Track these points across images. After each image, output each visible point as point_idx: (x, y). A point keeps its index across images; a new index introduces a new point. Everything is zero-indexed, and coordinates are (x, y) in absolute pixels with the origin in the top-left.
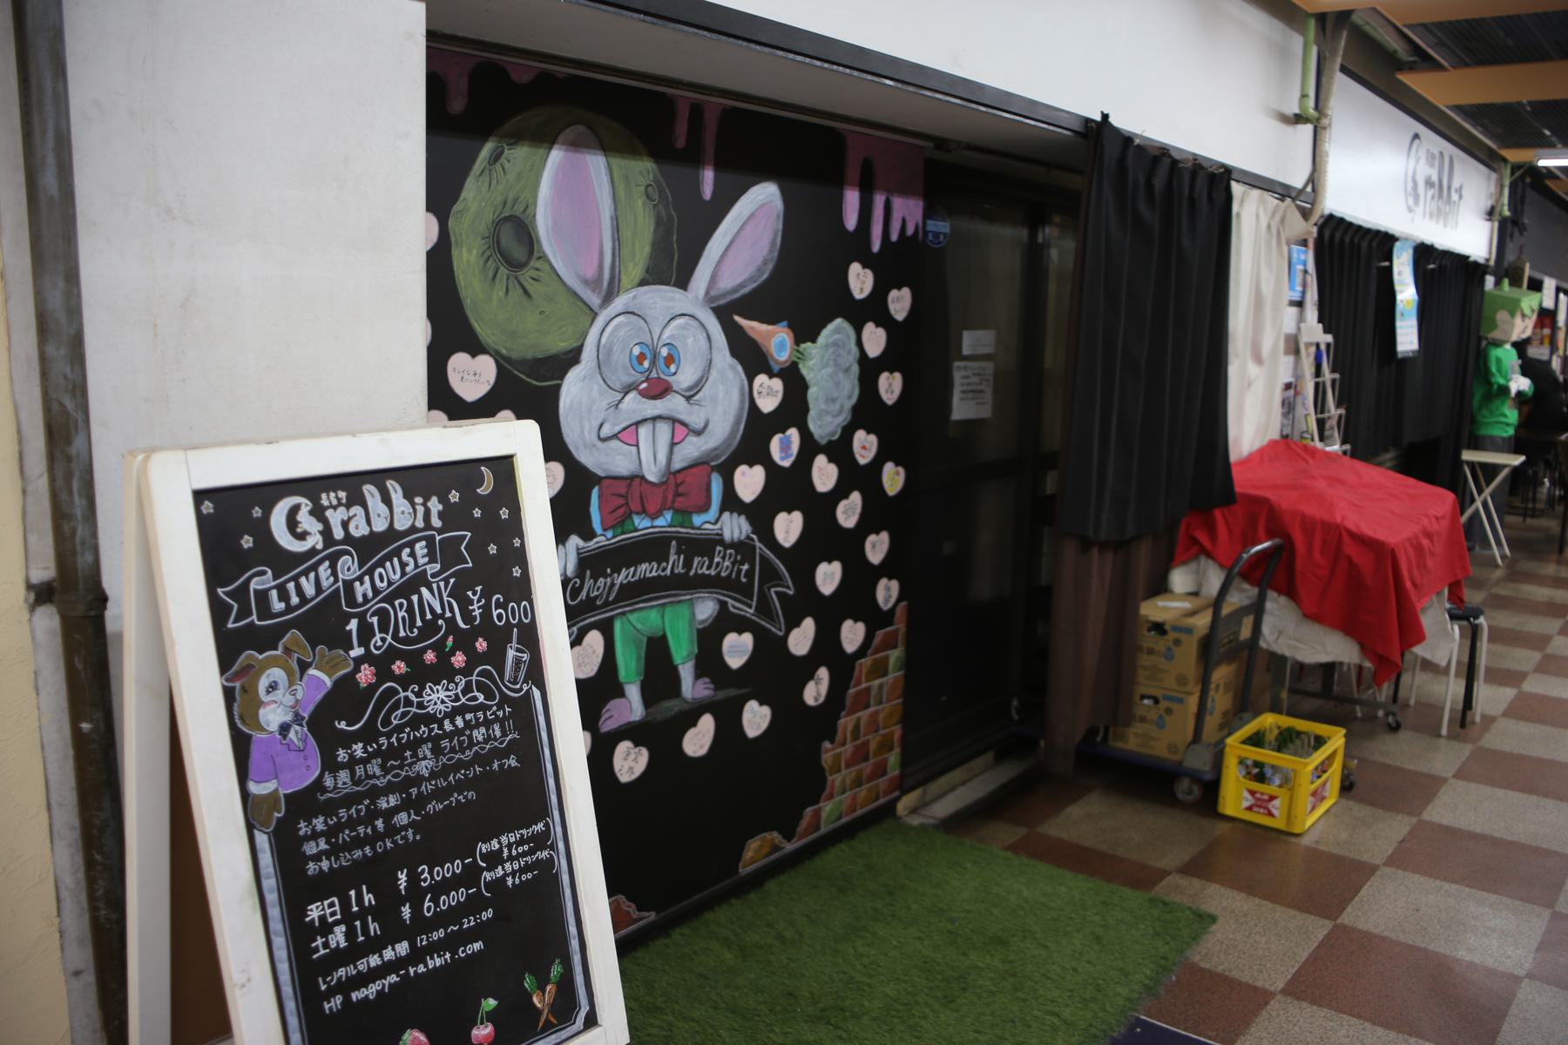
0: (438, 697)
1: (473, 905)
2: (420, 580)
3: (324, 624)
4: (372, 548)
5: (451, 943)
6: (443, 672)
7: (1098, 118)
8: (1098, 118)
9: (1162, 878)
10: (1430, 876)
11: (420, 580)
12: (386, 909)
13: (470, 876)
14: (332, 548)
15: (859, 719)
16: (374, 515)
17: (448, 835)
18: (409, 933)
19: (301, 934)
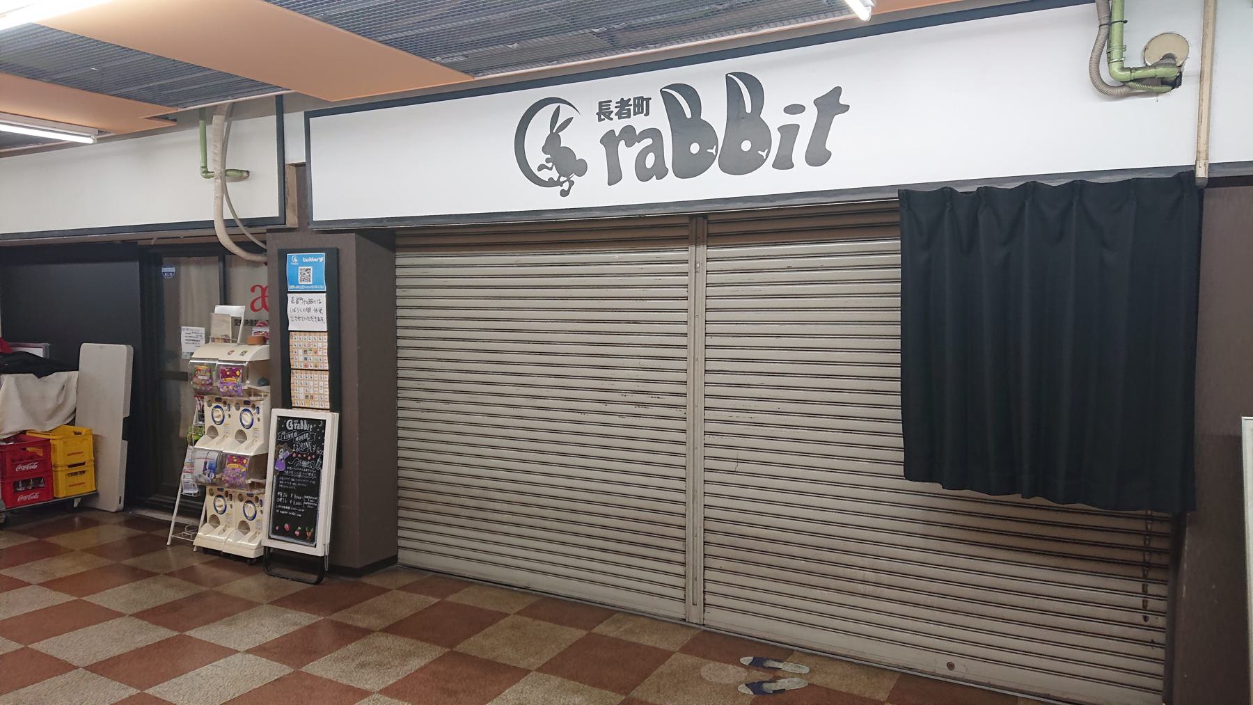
0: (304, 464)
1: (301, 507)
2: (305, 440)
3: (291, 443)
4: (301, 432)
5: (297, 512)
6: (306, 459)
7: (842, 101)
8: (842, 101)
9: (549, 663)
10: (828, 690)
11: (305, 440)
12: (289, 498)
13: (302, 501)
14: (294, 430)
15: (69, 380)
16: (305, 426)
17: (301, 491)
18: (292, 505)
19: (277, 496)
